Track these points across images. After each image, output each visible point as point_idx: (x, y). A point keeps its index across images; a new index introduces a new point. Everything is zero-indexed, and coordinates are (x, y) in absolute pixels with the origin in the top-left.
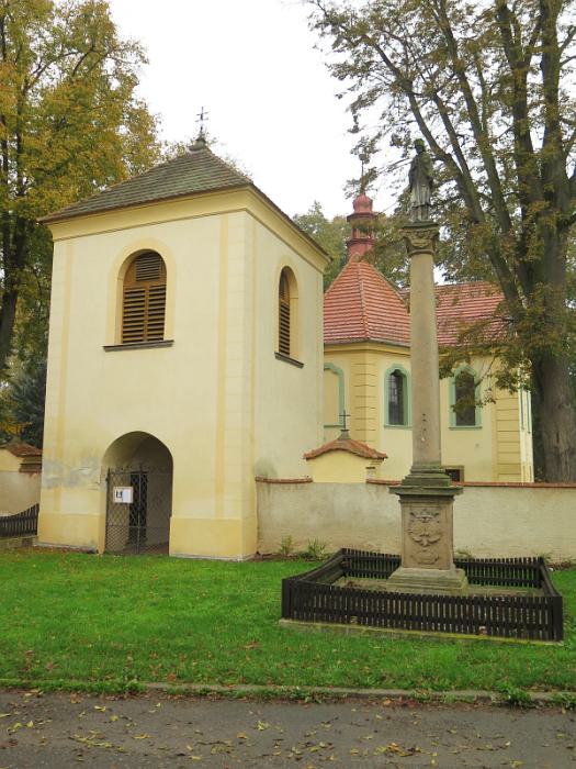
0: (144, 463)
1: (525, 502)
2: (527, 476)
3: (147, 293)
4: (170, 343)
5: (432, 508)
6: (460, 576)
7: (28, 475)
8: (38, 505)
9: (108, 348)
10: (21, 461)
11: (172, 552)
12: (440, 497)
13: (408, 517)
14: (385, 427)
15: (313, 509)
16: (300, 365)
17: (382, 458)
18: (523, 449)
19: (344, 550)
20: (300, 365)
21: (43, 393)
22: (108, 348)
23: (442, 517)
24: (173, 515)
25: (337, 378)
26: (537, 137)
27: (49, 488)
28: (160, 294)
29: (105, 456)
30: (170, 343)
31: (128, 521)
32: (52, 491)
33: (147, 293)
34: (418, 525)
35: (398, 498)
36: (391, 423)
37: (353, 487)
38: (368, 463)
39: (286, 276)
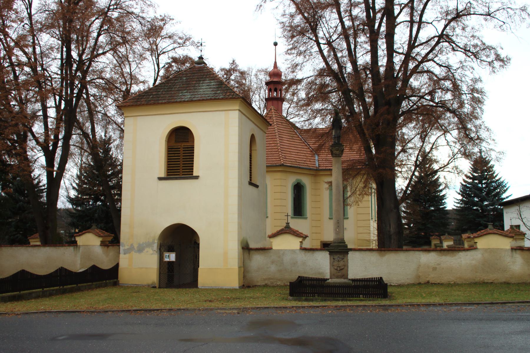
0: (181, 241)
1: (374, 257)
2: (374, 245)
3: (181, 149)
4: (197, 177)
5: (341, 256)
6: (351, 282)
7: (106, 248)
8: (117, 265)
9: (160, 179)
10: (101, 239)
11: (200, 285)
12: (344, 252)
13: (332, 260)
14: (292, 218)
15: (273, 262)
16: (257, 186)
17: (306, 237)
18: (372, 229)
19: (299, 277)
20: (257, 186)
21: (484, 249)
22: (160, 179)
23: (345, 260)
24: (200, 267)
25: (253, 182)
26: (383, 61)
27: (125, 254)
28: (191, 150)
29: (160, 237)
30: (197, 177)
31: (167, 271)
32: (127, 255)
33: (181, 149)
34: (336, 263)
35: (328, 253)
36: (294, 215)
37: (293, 251)
38: (301, 240)
39: (253, 138)
